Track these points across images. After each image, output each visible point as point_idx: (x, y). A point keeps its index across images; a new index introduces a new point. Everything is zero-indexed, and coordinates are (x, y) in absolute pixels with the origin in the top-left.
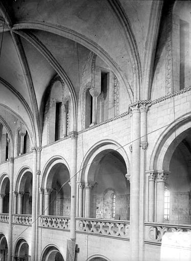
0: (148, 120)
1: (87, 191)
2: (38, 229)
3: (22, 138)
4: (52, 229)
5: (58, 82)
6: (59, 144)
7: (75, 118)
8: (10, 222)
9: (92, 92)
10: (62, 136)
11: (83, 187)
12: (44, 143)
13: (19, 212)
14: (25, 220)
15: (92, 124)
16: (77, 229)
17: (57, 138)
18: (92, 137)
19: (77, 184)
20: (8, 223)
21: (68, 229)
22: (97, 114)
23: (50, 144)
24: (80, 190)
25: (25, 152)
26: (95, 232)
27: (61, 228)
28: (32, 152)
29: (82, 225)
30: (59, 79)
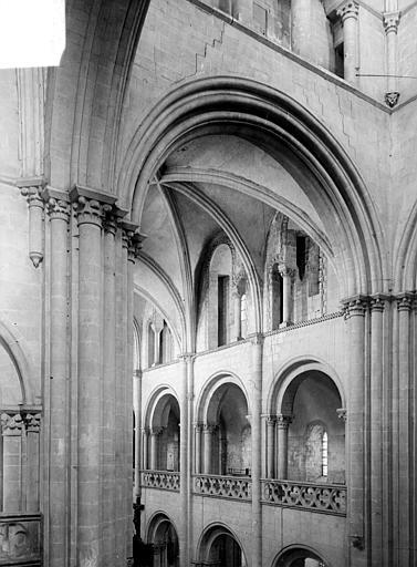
0: (264, 362)
1: (153, 439)
2: (191, 497)
3: (157, 336)
4: (219, 498)
5: (222, 246)
6: (224, 352)
7: (249, 310)
8: (255, 498)
9: (282, 268)
10: (232, 334)
11: (148, 434)
12: (201, 347)
13: (152, 466)
14: (159, 480)
15: (284, 325)
16: (195, 491)
17: (221, 342)
18: (285, 349)
19: (263, 420)
20: (250, 502)
21: (249, 498)
22: (291, 302)
23: (211, 350)
24: (270, 428)
25: (160, 362)
26: (290, 503)
27: (225, 495)
28: (178, 362)
29: (199, 484)
30: (226, 240)
